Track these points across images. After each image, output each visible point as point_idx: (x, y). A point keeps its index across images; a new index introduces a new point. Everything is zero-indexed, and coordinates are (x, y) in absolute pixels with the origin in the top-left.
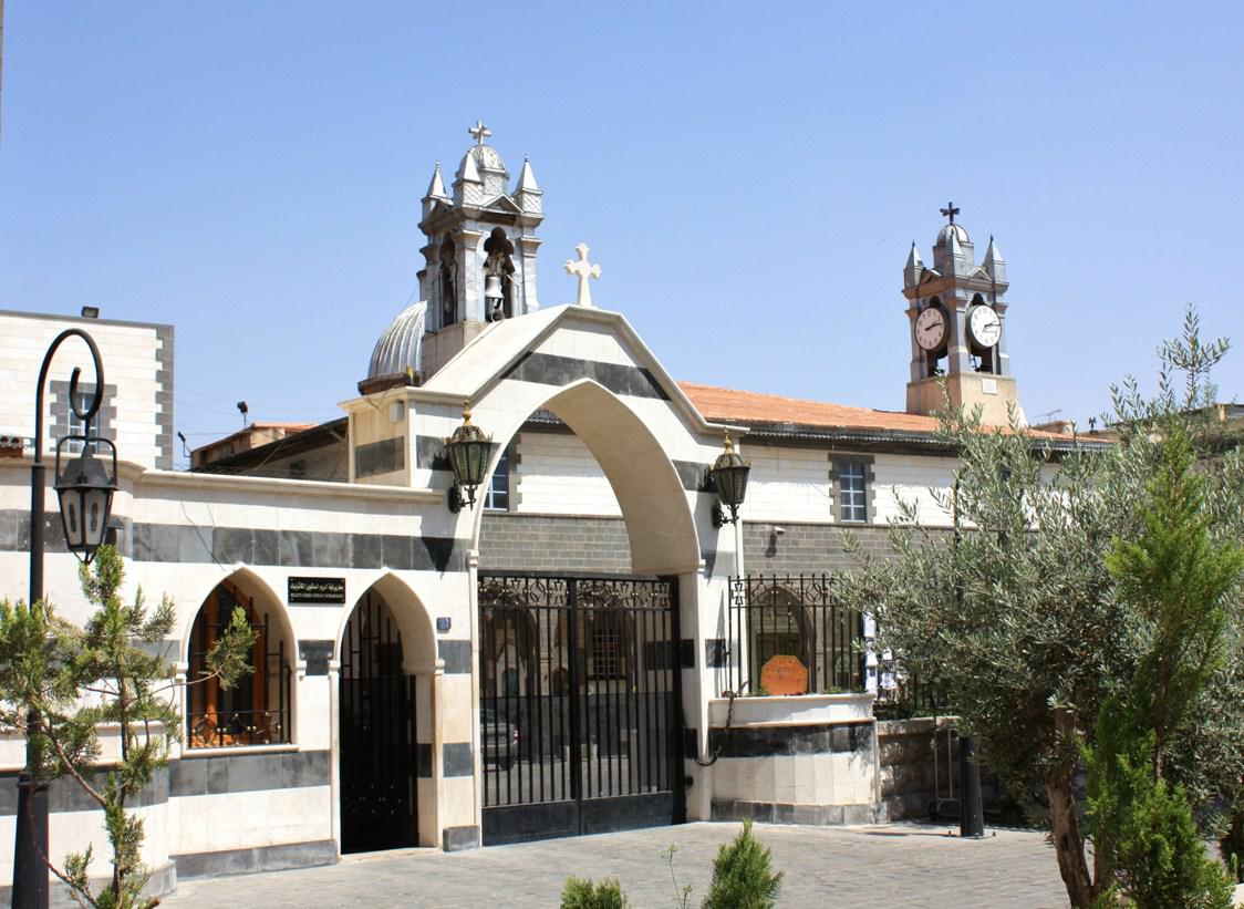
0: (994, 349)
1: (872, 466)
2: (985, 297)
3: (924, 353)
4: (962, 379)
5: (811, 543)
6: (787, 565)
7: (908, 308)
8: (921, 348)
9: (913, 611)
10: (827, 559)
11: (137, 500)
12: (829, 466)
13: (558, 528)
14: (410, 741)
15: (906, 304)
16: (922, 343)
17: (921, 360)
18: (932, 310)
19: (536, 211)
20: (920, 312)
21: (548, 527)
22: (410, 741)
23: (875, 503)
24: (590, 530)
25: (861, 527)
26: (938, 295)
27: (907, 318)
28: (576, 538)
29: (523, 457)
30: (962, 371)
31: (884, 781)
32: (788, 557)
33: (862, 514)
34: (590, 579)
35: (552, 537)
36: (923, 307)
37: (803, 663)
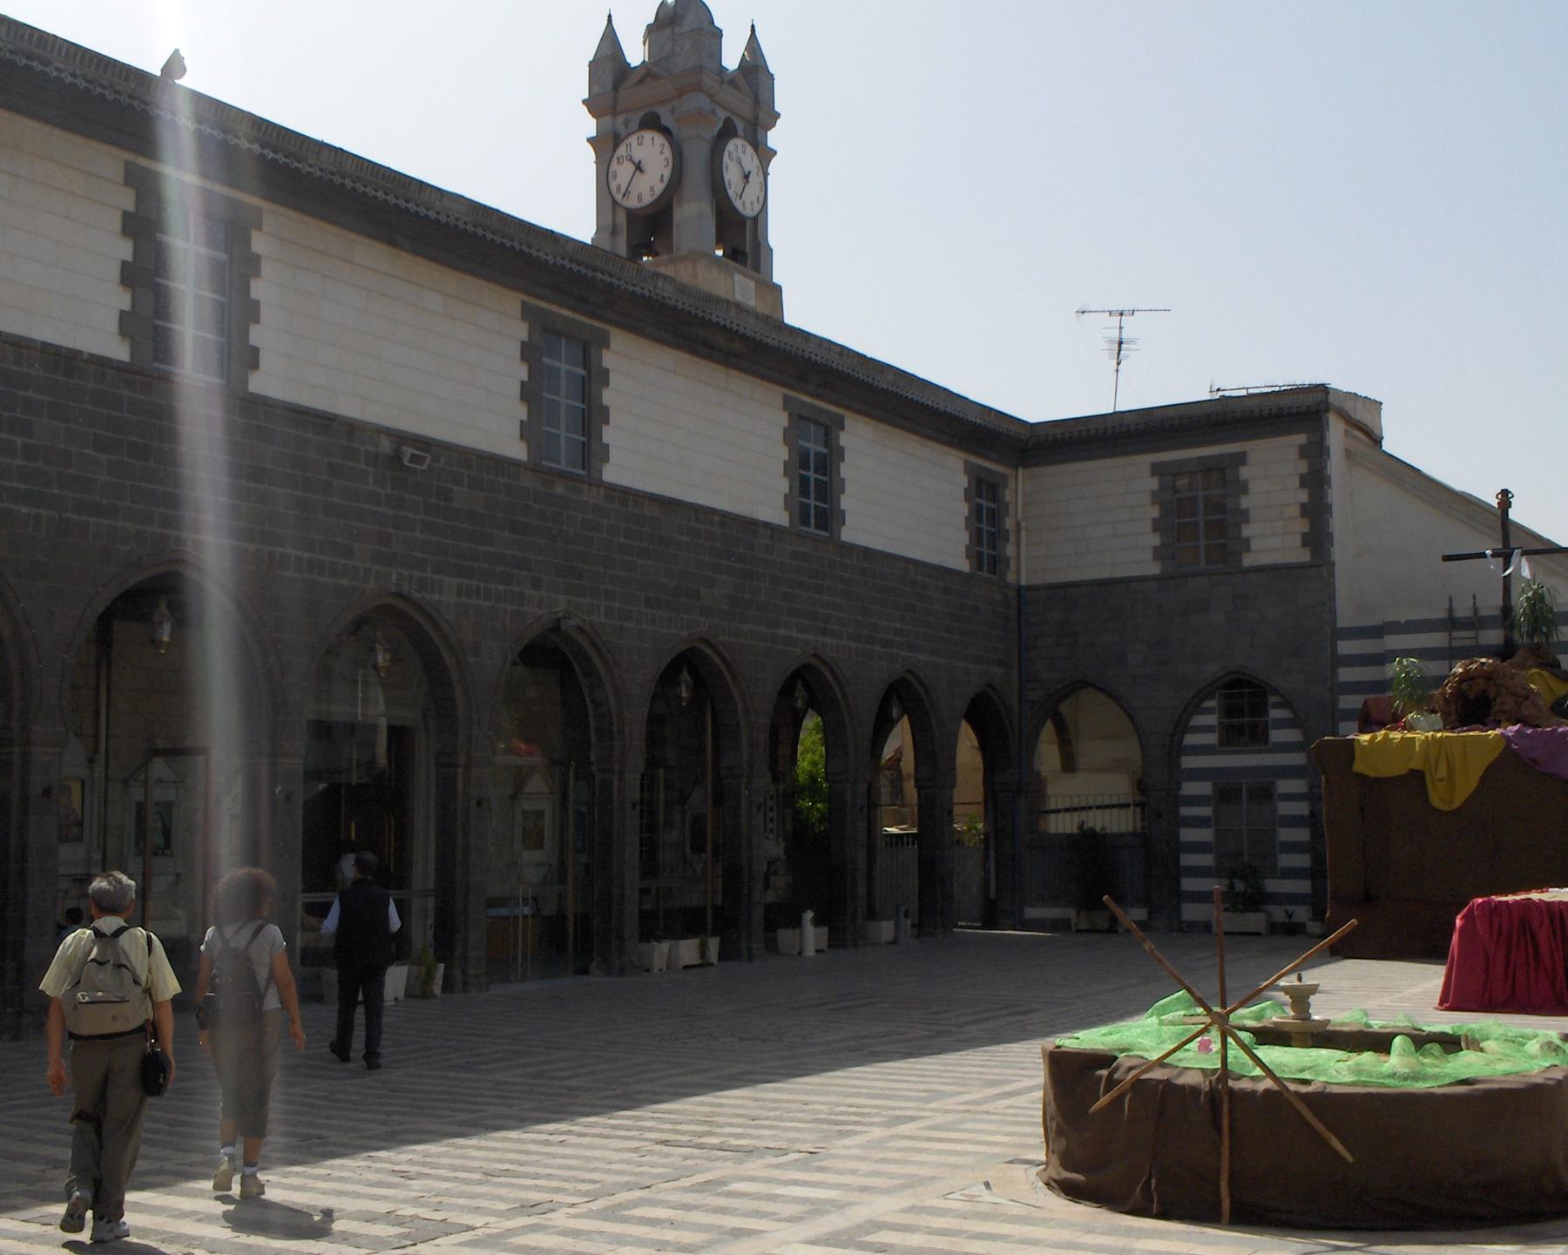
0: (749, 224)
1: (605, 353)
2: (740, 126)
3: (622, 219)
7: (593, 133)
8: (614, 202)
9: (1512, 678)
11: (779, 112)
15: (590, 126)
18: (648, 135)
20: (617, 140)
25: (580, 479)
30: (1111, 411)
31: (1485, 553)
36: (623, 132)
37: (65, 1243)
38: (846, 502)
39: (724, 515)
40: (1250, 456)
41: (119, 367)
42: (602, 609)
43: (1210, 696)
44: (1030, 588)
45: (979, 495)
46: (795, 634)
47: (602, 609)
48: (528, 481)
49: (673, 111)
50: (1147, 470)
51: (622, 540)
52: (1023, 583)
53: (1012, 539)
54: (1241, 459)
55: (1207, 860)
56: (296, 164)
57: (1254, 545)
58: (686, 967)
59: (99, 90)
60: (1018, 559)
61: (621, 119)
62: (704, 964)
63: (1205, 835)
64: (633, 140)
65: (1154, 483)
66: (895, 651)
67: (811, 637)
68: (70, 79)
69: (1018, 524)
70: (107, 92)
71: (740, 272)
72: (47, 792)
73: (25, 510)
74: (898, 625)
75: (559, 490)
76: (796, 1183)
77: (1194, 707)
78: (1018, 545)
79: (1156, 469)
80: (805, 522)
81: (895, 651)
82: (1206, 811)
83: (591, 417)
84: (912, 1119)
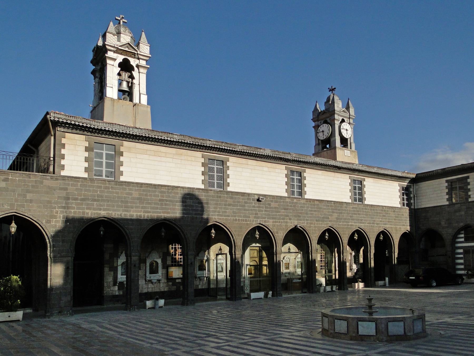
0: (349, 140)
2: (346, 119)
3: (320, 142)
4: (337, 149)
5: (276, 205)
6: (265, 214)
8: (319, 139)
10: (284, 212)
12: (286, 172)
13: (144, 191)
14: (342, 260)
16: (320, 138)
17: (319, 144)
18: (324, 125)
19: (146, 52)
20: (318, 126)
21: (138, 190)
22: (342, 260)
23: (306, 189)
24: (162, 192)
26: (327, 119)
27: (313, 129)
28: (155, 196)
29: (124, 153)
32: (265, 211)
33: (300, 194)
34: (362, 339)
35: (140, 194)
38: (365, 196)
39: (334, 202)
40: (470, 177)
41: (202, 190)
42: (306, 223)
43: (462, 231)
44: (417, 209)
45: (355, 183)
46: (353, 224)
47: (306, 223)
48: (288, 200)
49: (330, 119)
50: (445, 182)
51: (310, 209)
52: (416, 208)
53: (413, 199)
54: (468, 177)
55: (462, 267)
56: (234, 149)
57: (471, 196)
58: (328, 291)
59: (195, 143)
60: (414, 203)
61: (319, 122)
62: (332, 291)
63: (462, 261)
64: (322, 126)
65: (446, 184)
66: (380, 225)
67: (358, 224)
68: (189, 142)
69: (414, 195)
70: (196, 143)
71: (346, 150)
72: (191, 263)
73: (185, 216)
74: (381, 220)
75: (295, 201)
76: (299, 340)
77: (458, 232)
78: (414, 200)
79: (447, 181)
80: (355, 200)
81: (380, 225)
82: (462, 256)
83: (301, 187)
84: (184, 352)
